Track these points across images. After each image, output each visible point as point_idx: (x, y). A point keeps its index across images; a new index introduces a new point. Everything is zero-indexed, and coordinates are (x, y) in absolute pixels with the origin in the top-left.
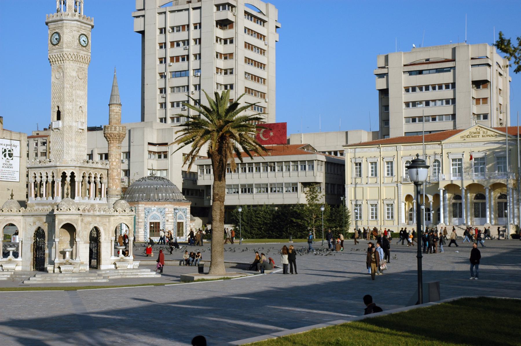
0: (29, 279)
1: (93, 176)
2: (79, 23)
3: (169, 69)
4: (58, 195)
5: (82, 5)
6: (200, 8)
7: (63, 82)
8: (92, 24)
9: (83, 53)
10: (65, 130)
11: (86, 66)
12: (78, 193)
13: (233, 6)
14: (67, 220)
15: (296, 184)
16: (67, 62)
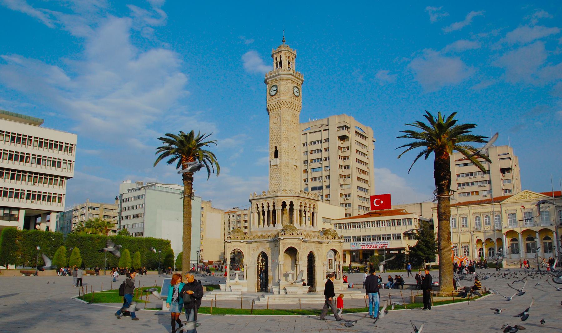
0: (259, 300)
1: (308, 205)
2: (293, 77)
3: (310, 167)
4: (279, 222)
5: (294, 65)
6: (328, 129)
7: (280, 125)
8: (303, 79)
9: (296, 102)
10: (282, 166)
11: (298, 113)
12: (297, 220)
13: (348, 128)
14: (290, 243)
15: (400, 234)
16: (284, 109)
